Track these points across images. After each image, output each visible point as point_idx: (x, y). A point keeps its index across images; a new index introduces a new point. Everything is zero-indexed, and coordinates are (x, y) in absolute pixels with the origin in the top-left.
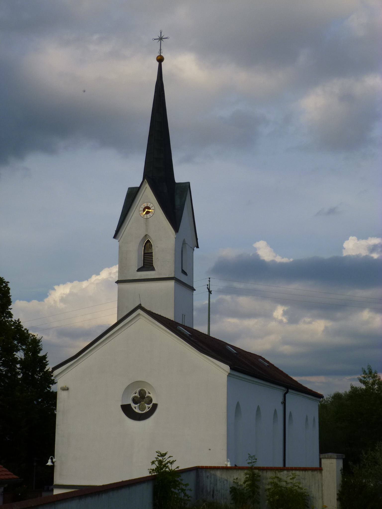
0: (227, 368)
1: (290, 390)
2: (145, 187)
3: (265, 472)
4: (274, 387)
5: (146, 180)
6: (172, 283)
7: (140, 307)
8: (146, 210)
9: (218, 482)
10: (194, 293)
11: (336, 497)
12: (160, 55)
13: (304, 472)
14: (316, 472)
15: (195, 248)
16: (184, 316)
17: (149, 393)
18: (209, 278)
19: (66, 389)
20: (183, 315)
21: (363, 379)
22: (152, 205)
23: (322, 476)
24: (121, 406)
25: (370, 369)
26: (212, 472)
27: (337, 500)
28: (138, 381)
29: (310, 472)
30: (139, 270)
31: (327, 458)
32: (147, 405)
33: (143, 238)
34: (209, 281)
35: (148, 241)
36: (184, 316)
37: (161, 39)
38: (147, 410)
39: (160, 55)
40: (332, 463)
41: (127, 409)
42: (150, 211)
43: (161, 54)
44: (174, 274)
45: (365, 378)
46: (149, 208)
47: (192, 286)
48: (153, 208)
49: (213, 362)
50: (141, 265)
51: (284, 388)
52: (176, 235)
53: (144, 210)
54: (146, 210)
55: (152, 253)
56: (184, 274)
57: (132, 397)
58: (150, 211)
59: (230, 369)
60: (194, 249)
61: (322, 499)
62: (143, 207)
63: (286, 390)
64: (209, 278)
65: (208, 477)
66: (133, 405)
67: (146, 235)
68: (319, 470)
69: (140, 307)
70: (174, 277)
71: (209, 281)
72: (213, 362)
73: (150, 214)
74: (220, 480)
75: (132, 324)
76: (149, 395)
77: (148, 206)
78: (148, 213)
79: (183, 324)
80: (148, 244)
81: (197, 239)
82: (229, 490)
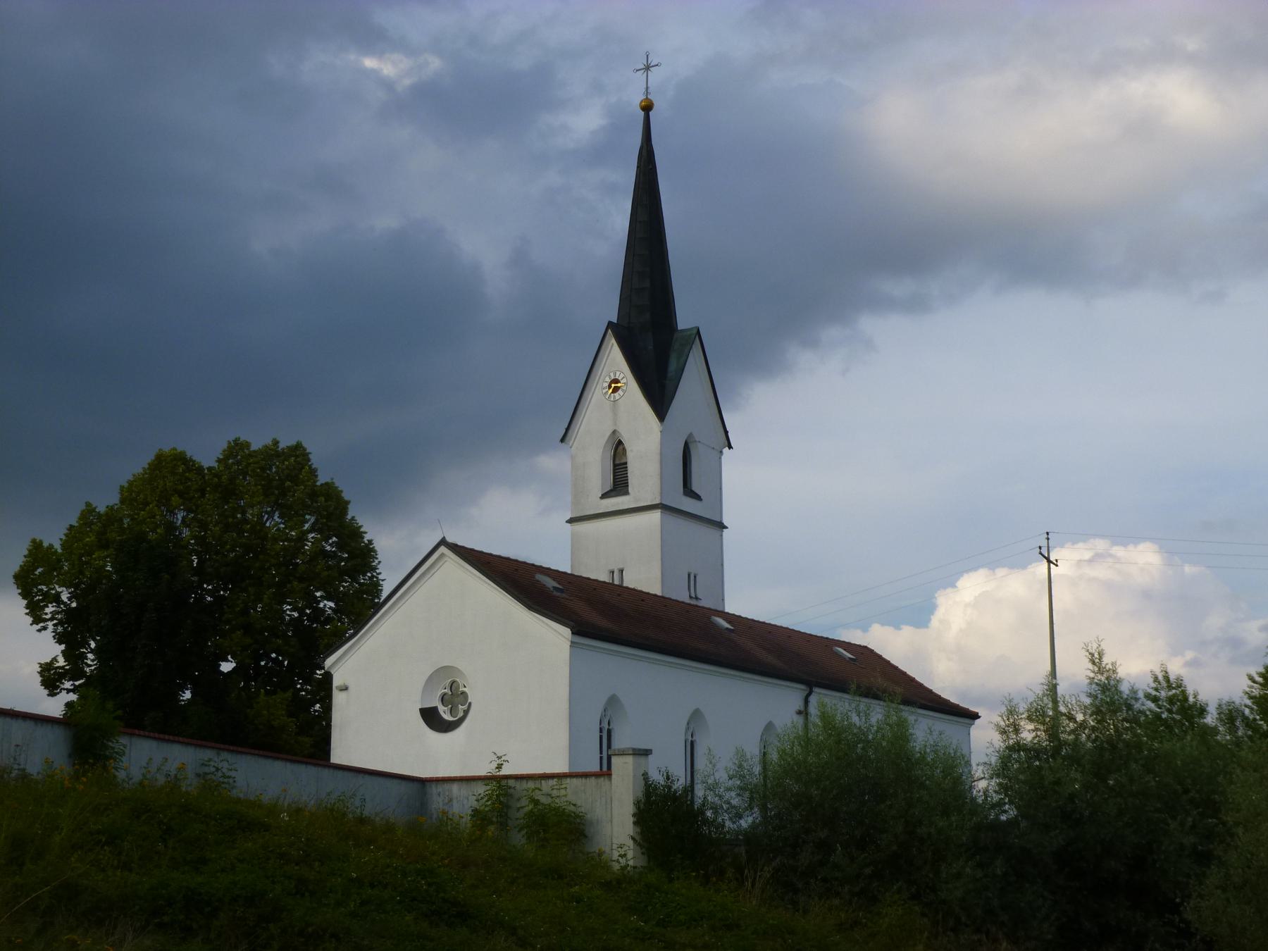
0: (566, 632)
1: (816, 690)
2: (611, 344)
3: (525, 781)
4: (749, 679)
5: (610, 331)
6: (656, 516)
7: (443, 542)
8: (613, 385)
9: (455, 801)
10: (724, 533)
11: (632, 820)
12: (647, 98)
13: (583, 779)
14: (602, 779)
15: (726, 450)
16: (692, 579)
17: (465, 687)
18: (1048, 533)
19: (344, 689)
20: (689, 575)
21: (1154, 693)
22: (622, 375)
23: (611, 783)
24: (420, 709)
25: (1166, 672)
26: (447, 786)
27: (635, 823)
28: (442, 667)
29: (593, 780)
30: (604, 496)
31: (618, 755)
32: (460, 707)
33: (609, 437)
34: (1048, 539)
35: (620, 443)
36: (692, 579)
37: (648, 68)
38: (461, 714)
39: (647, 98)
40: (626, 763)
41: (430, 717)
42: (619, 385)
43: (649, 97)
44: (659, 498)
45: (1156, 690)
46: (616, 381)
47: (719, 521)
48: (624, 381)
49: (547, 624)
50: (608, 487)
51: (803, 687)
52: (661, 425)
53: (610, 387)
54: (613, 385)
55: (626, 463)
56: (691, 497)
57: (440, 694)
58: (619, 385)
59: (572, 633)
60: (721, 452)
61: (612, 822)
62: (608, 380)
63: (808, 689)
64: (1048, 533)
65: (439, 795)
66: (441, 709)
67: (614, 432)
68: (608, 775)
69: (443, 542)
70: (661, 504)
71: (1048, 539)
72: (547, 624)
73: (620, 392)
74: (457, 798)
75: (433, 571)
76: (464, 689)
77: (617, 377)
78: (616, 390)
79: (616, 582)
80: (621, 447)
81: (726, 432)
82: (470, 812)
